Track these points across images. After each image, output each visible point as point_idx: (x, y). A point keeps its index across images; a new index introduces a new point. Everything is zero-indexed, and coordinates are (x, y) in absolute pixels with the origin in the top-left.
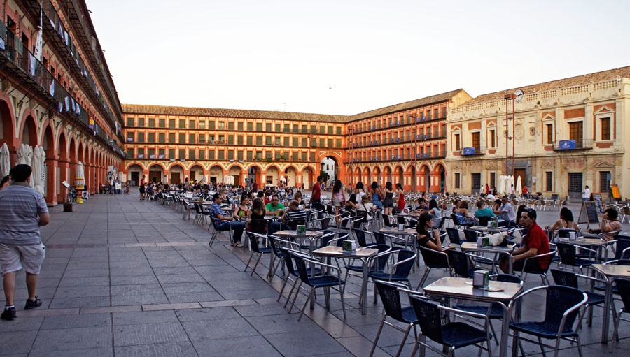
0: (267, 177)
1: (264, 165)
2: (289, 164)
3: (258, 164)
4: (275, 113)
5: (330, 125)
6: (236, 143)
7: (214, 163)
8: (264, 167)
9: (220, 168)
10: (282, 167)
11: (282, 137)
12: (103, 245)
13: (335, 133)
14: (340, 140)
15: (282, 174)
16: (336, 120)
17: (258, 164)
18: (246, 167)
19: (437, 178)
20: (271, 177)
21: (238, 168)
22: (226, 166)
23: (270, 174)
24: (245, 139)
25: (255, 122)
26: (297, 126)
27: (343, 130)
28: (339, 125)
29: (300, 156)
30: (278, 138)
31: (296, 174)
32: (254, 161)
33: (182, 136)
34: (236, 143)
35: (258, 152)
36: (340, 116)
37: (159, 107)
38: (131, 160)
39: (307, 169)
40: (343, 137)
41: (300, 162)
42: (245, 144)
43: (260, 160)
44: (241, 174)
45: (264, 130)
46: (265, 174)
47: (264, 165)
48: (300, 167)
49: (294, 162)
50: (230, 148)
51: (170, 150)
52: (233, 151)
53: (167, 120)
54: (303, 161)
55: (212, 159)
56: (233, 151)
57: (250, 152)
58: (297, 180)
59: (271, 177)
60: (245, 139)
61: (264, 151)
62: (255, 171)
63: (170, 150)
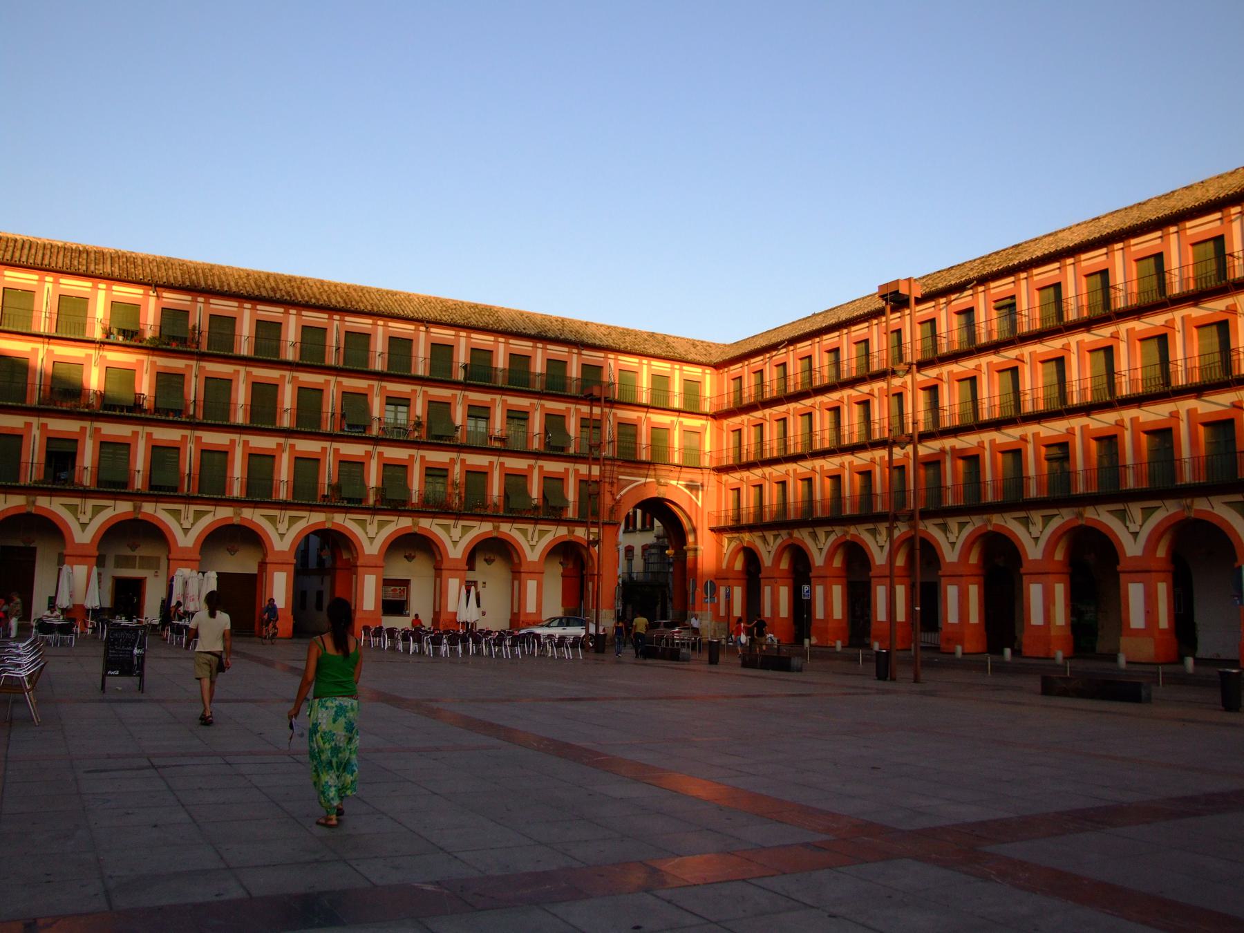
0: (387, 583)
1: (372, 529)
2: (484, 528)
3: (345, 522)
4: (116, 257)
5: (661, 367)
6: (240, 418)
7: (405, 522)
8: (371, 535)
9: (155, 533)
10: (456, 539)
11: (500, 406)
12: (922, 648)
13: (421, 369)
14: (698, 432)
15: (455, 570)
16: (681, 351)
17: (345, 522)
18: (284, 533)
19: (837, 591)
20: (406, 583)
21: (249, 537)
22: (186, 526)
23: (399, 569)
24: (288, 398)
25: (336, 328)
26: (563, 364)
27: (708, 390)
28: (693, 372)
29: (496, 489)
30: (479, 412)
31: (438, 570)
32: (327, 506)
33: (264, 395)
34: (240, 418)
35: (352, 468)
36: (694, 344)
37: (476, 306)
38: (116, 496)
39: (565, 551)
40: (709, 423)
41: (536, 521)
42: (286, 422)
43: (354, 504)
44: (263, 565)
45: (378, 365)
46: (373, 567)
47: (456, 533)
48: (533, 542)
49: (346, 510)
50: (212, 438)
51: (106, 445)
52: (224, 454)
53: (380, 334)
54: (550, 512)
55: (112, 485)
56: (224, 454)
57: (306, 466)
58: (517, 598)
59: (406, 583)
60: (288, 398)
61: (284, 458)
62: (326, 558)
63: (106, 445)
